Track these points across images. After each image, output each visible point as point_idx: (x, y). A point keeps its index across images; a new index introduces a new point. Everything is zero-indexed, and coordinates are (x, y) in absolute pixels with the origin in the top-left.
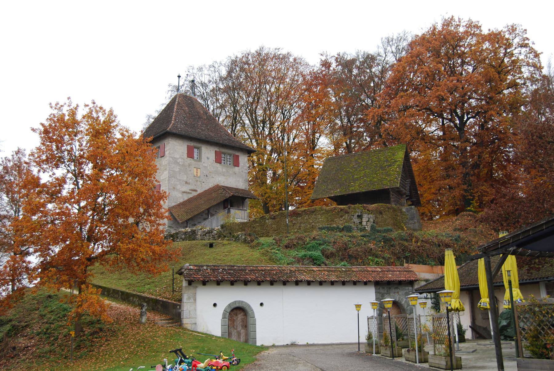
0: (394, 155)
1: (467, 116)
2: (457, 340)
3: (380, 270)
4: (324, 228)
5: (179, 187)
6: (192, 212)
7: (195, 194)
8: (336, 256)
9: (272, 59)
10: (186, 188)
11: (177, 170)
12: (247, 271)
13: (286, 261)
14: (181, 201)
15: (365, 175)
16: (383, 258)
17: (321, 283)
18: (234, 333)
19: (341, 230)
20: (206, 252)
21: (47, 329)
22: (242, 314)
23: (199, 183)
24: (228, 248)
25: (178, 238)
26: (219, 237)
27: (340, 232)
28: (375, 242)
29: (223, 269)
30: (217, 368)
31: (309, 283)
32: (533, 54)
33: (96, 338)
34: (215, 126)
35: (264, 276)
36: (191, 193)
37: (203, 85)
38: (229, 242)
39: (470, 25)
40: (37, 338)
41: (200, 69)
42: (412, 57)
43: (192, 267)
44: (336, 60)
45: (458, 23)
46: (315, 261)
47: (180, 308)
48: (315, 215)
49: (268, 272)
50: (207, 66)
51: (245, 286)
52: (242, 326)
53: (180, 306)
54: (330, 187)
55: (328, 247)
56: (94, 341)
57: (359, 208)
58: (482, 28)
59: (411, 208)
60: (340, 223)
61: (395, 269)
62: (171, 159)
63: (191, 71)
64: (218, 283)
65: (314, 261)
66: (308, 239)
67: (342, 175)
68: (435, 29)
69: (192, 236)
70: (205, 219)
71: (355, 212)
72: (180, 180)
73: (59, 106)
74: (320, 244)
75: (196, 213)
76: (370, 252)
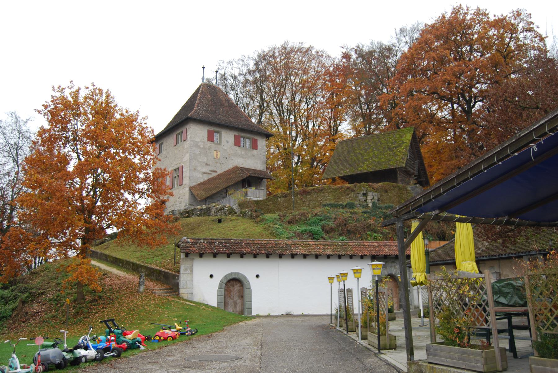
0: (402, 137)
1: (475, 100)
2: (422, 315)
3: (376, 244)
4: (327, 205)
5: (199, 168)
6: (211, 191)
7: (215, 174)
8: (335, 231)
9: (296, 52)
10: (205, 170)
11: (198, 153)
12: (243, 244)
13: (286, 236)
14: (202, 181)
15: (374, 156)
16: (382, 233)
17: (317, 257)
18: (230, 302)
19: (344, 207)
20: (214, 227)
21: (58, 297)
22: (239, 285)
23: (218, 164)
24: (234, 223)
25: (193, 214)
26: (230, 213)
27: (343, 208)
28: (375, 218)
29: (219, 243)
30: (160, 339)
31: (305, 256)
32: (538, 38)
33: (94, 305)
34: (236, 112)
35: (260, 249)
36: (211, 174)
37: (235, 78)
38: (237, 218)
39: (478, 12)
40: (48, 304)
41: (230, 63)
42: (419, 44)
43: (189, 240)
44: (356, 51)
45: (466, 11)
46: (314, 236)
47: (178, 279)
48: (323, 193)
49: (265, 246)
50: (237, 60)
51: (241, 259)
52: (239, 297)
53: (178, 276)
54: (340, 167)
55: (329, 223)
56: (91, 309)
57: (364, 187)
58: (489, 16)
59: (416, 187)
60: (346, 200)
61: (392, 244)
62: (192, 143)
63: (221, 64)
64: (215, 255)
65: (313, 235)
66: (310, 215)
67: (352, 156)
68: (444, 17)
69: (207, 212)
70: (224, 198)
71: (361, 191)
72: (200, 162)
73: (61, 89)
74: (321, 220)
75: (214, 192)
76: (369, 227)
